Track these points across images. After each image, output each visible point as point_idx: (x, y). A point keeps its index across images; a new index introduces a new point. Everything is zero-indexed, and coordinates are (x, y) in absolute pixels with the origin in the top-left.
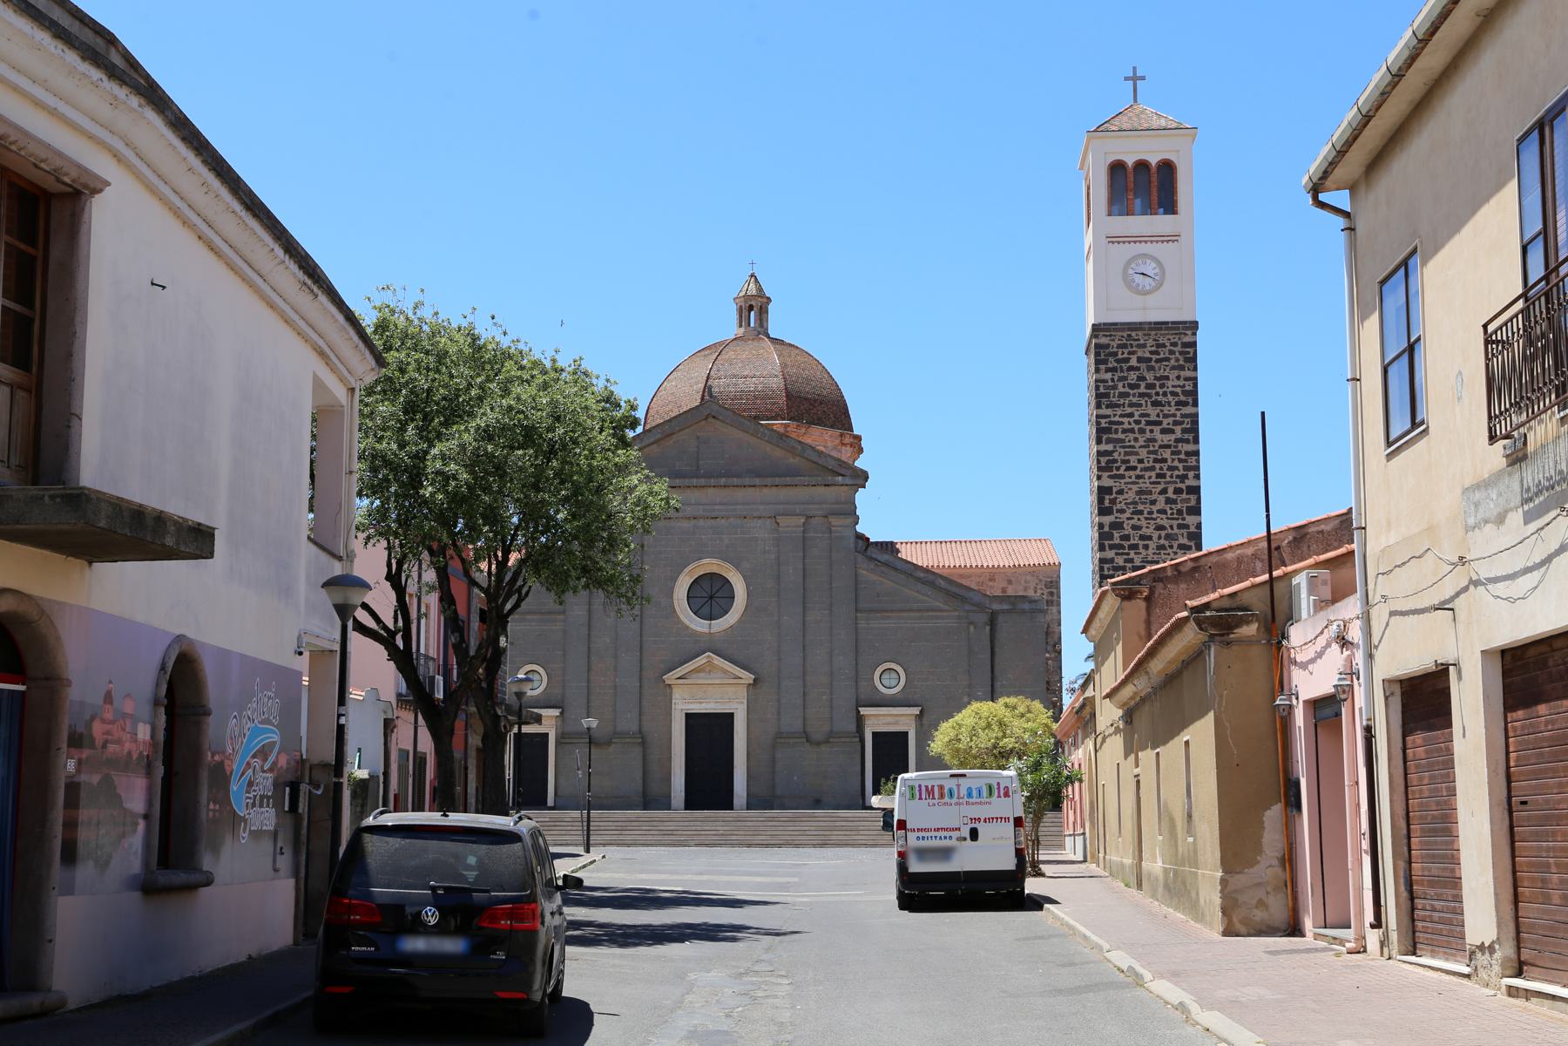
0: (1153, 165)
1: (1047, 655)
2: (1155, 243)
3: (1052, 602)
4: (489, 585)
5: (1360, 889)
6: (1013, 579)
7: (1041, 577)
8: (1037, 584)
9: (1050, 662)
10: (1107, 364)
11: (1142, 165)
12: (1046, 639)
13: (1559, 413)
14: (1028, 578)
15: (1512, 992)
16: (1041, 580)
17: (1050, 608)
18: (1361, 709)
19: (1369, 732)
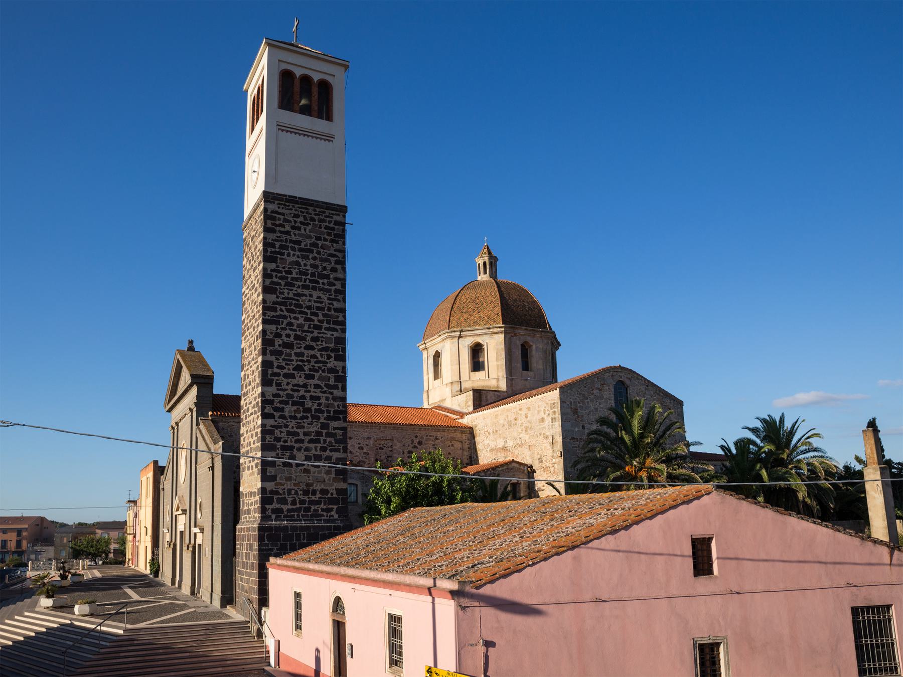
0: (298, 77)
1: (554, 460)
2: (314, 139)
3: (555, 418)
4: (621, 432)
5: (242, 645)
6: (531, 407)
7: (548, 402)
8: (545, 407)
9: (556, 466)
10: (295, 334)
11: (306, 79)
12: (553, 448)
13: (247, 447)
14: (540, 403)
15: (334, 135)
16: (547, 404)
17: (554, 423)
18: (182, 533)
19: (160, 602)
